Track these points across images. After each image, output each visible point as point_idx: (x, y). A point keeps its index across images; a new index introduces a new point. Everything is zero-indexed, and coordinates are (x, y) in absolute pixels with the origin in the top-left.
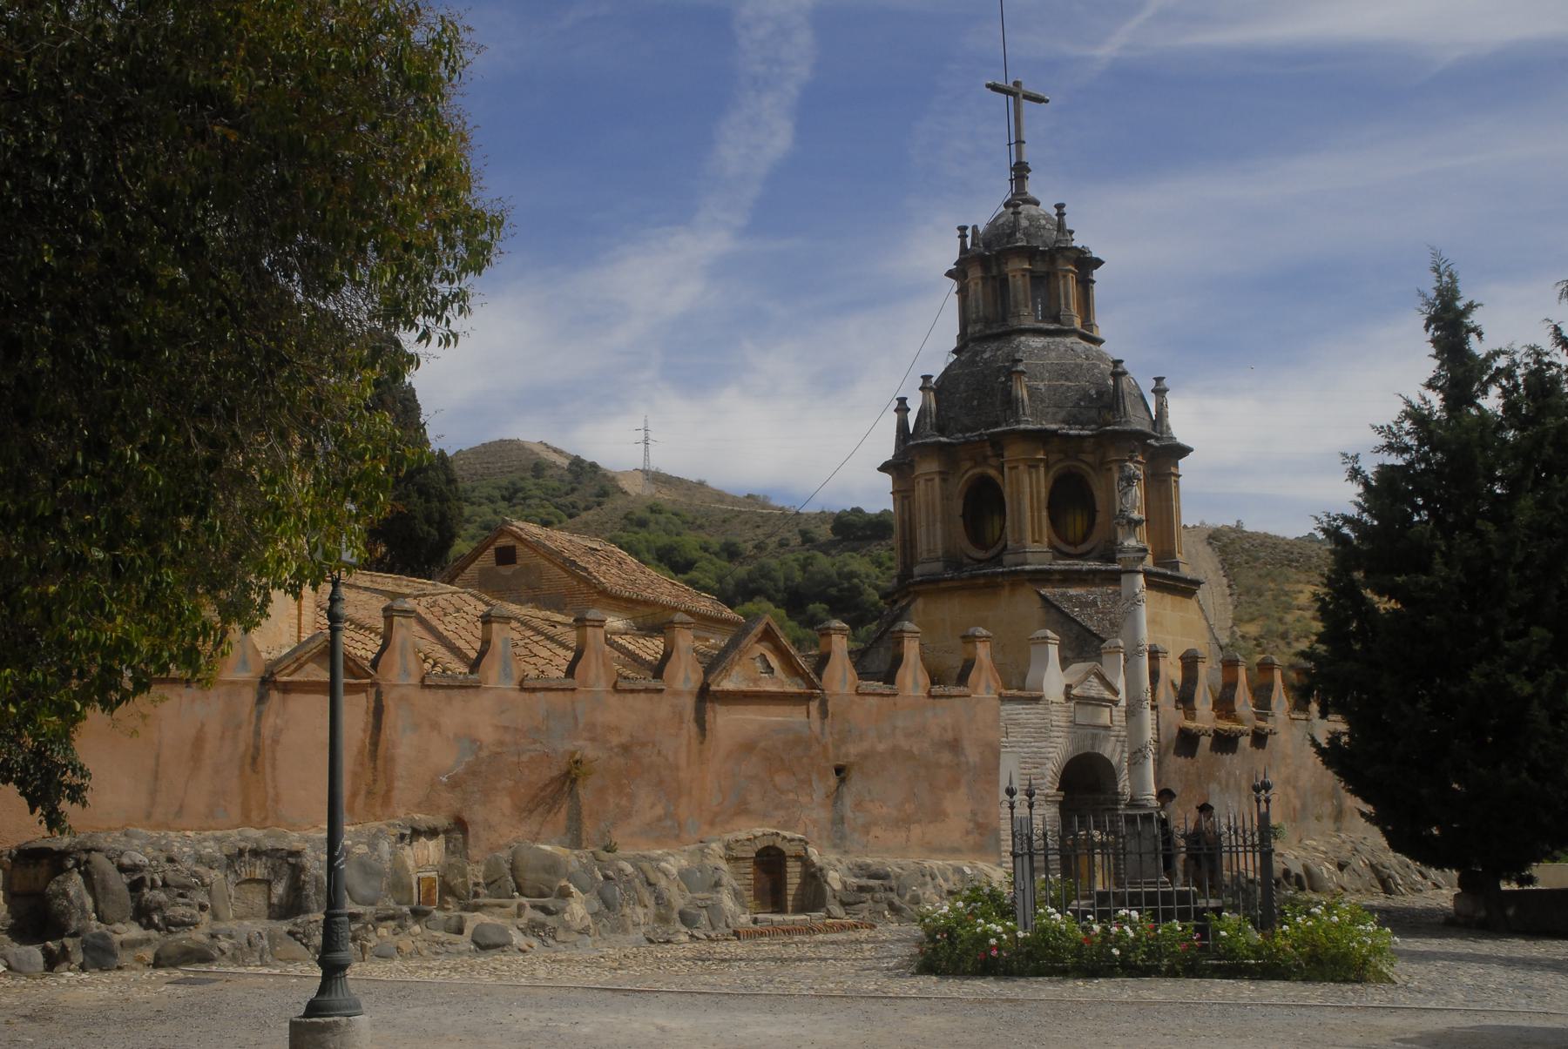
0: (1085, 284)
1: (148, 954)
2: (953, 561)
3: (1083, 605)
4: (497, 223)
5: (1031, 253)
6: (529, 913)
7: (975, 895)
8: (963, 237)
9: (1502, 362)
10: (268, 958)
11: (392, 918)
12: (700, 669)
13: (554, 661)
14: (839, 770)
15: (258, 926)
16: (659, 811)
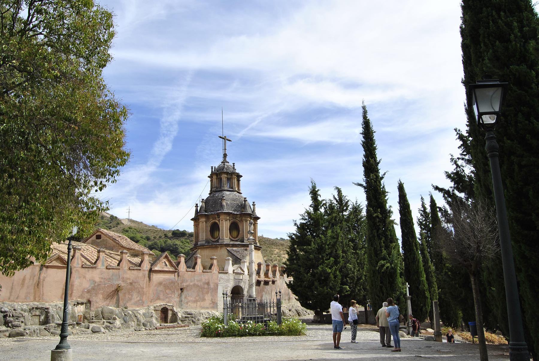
0: (238, 181)
1: (7, 334)
2: (207, 241)
3: (237, 252)
4: (128, 155)
5: (227, 173)
6: (106, 324)
7: (213, 318)
8: (212, 169)
9: (324, 202)
10: (39, 335)
11: (71, 325)
12: (150, 264)
13: (114, 263)
14: (181, 289)
15: (37, 327)
16: (138, 299)
